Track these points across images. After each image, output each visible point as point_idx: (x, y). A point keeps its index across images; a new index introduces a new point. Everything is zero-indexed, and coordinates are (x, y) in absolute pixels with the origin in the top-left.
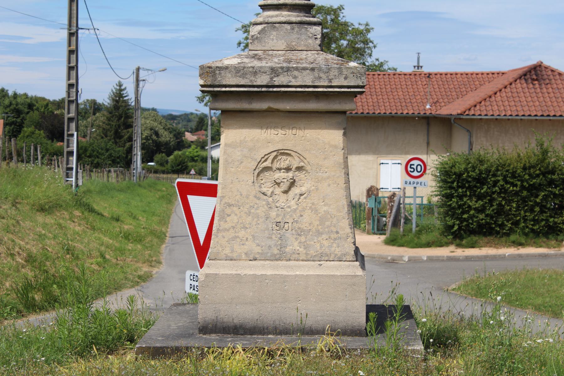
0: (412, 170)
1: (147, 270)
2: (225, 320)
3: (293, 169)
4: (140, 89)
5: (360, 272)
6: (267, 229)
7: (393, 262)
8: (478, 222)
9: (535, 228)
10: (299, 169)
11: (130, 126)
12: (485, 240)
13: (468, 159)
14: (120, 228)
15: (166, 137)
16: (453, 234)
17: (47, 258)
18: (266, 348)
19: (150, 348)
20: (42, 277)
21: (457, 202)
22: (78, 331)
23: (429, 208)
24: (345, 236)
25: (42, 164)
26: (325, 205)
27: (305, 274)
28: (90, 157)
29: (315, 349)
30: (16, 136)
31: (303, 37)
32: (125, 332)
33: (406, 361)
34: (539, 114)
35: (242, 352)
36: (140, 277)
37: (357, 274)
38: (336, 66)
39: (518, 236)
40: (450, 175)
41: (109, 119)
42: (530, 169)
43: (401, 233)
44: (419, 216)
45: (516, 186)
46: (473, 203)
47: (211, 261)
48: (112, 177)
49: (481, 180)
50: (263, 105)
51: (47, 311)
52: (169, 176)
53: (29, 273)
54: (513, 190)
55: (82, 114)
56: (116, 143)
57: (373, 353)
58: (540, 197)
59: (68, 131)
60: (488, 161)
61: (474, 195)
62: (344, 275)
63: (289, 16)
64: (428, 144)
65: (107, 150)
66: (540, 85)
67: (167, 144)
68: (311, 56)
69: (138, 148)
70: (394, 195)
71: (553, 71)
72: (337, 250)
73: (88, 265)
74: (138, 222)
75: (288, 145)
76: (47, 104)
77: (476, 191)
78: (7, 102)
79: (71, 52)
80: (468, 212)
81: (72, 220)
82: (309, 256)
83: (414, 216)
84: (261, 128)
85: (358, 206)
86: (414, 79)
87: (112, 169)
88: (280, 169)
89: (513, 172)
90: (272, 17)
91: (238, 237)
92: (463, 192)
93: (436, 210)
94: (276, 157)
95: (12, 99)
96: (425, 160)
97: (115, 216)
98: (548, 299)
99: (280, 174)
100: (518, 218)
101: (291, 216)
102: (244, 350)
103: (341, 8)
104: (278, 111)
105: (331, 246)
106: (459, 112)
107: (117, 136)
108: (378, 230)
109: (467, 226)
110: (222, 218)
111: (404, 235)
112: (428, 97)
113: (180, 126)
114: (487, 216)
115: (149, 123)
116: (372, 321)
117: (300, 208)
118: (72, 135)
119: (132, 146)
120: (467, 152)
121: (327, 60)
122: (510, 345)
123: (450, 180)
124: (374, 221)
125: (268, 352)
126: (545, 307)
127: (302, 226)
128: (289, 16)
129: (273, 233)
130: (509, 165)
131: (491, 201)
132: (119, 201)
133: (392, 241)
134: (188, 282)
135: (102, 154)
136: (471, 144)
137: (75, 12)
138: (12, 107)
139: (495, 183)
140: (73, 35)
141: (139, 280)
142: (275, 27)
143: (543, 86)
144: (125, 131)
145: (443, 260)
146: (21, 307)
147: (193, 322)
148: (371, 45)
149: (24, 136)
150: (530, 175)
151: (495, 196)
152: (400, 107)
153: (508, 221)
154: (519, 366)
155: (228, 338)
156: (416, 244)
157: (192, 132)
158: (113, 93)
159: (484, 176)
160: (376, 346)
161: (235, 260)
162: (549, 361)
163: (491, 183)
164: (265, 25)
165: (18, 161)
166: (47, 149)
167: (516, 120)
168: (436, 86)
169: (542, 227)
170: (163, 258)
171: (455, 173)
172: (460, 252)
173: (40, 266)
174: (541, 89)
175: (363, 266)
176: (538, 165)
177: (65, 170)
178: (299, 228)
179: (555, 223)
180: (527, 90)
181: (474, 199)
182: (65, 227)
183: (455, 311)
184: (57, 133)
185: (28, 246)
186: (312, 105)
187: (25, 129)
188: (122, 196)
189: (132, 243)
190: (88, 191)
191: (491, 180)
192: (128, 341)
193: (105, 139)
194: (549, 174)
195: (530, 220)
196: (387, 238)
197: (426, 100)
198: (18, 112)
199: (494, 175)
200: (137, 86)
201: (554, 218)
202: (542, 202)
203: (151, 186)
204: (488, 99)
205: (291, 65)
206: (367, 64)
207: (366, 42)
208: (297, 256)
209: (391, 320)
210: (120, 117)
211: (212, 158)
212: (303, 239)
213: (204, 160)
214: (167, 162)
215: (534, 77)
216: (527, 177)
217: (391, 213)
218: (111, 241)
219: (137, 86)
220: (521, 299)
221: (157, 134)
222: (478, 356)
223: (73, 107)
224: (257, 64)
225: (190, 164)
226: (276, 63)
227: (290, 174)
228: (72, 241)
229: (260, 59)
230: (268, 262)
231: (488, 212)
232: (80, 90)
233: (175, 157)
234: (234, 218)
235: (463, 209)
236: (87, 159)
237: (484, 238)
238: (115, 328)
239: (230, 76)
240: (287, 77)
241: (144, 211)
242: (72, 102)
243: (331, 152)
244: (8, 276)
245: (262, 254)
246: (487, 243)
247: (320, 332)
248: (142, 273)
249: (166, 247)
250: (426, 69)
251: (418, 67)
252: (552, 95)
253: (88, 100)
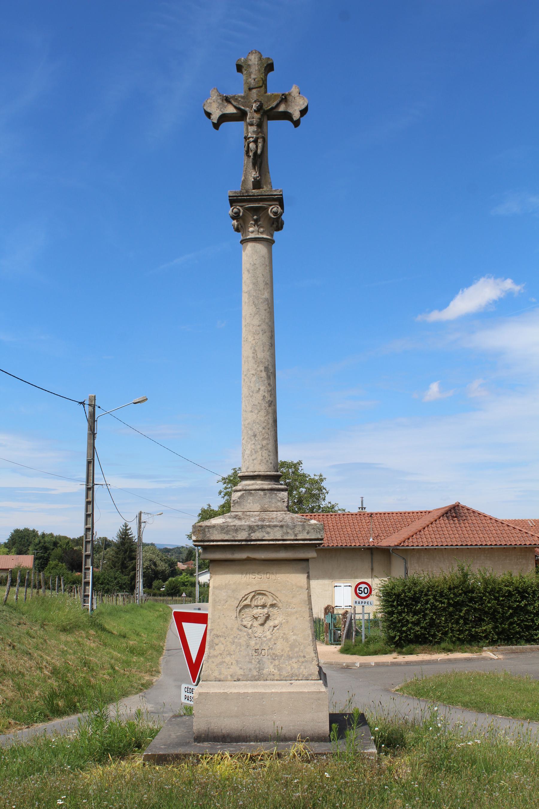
0: (360, 592)
1: (148, 678)
2: (215, 730)
3: (268, 606)
4: (142, 529)
5: (323, 689)
6: (248, 655)
7: (348, 667)
8: (414, 633)
9: (461, 637)
10: (272, 606)
11: (135, 559)
12: (421, 647)
13: (404, 583)
14: (127, 643)
15: (162, 566)
16: (395, 643)
17: (68, 670)
18: (249, 754)
19: (155, 755)
20: (65, 687)
21: (397, 618)
22: (96, 740)
23: (375, 622)
24: (310, 659)
25: (65, 590)
26: (294, 635)
27: (279, 691)
28: (102, 584)
30: (43, 568)
31: (274, 501)
32: (134, 739)
33: (363, 764)
35: (230, 758)
36: (143, 685)
37: (321, 690)
38: (300, 523)
39: (447, 644)
40: (390, 596)
41: (117, 553)
42: (454, 589)
45: (444, 603)
47: (203, 682)
48: (119, 600)
49: (415, 599)
50: (243, 555)
51: (68, 715)
52: (165, 598)
53: (54, 683)
54: (442, 607)
55: (96, 549)
56: (122, 572)
57: (336, 757)
58: (463, 612)
59: (85, 565)
60: (421, 583)
61: (411, 611)
62: (311, 692)
64: (372, 569)
65: (116, 578)
67: (163, 572)
68: (280, 515)
69: (141, 576)
70: (346, 612)
71: (468, 509)
72: (305, 671)
73: (101, 675)
74: (140, 638)
75: (263, 587)
77: (412, 608)
78: (37, 541)
79: (88, 503)
81: (88, 637)
82: (282, 677)
83: (363, 629)
84: (242, 573)
85: (317, 622)
86: (359, 518)
87: (120, 594)
88: (257, 606)
89: (441, 592)
90: (249, 485)
92: (401, 609)
93: (381, 624)
94: (254, 596)
95: (41, 538)
96: (370, 583)
97: (122, 634)
98: (473, 697)
99: (257, 610)
100: (447, 629)
101: (267, 644)
102: (231, 756)
103: (300, 463)
104: (255, 559)
105: (300, 668)
106: (396, 544)
107: (124, 566)
108: (334, 641)
109: (406, 636)
110: (212, 647)
111: (356, 645)
112: (371, 532)
113: (173, 557)
114: (421, 628)
115: (149, 555)
116: (334, 730)
117: (274, 638)
118: (89, 569)
121: (292, 519)
122: (447, 747)
126: (472, 704)
127: (276, 653)
128: (262, 484)
129: (253, 658)
130: (438, 586)
131: (425, 616)
132: (125, 621)
133: (346, 650)
134: (183, 694)
138: (41, 545)
139: (427, 601)
140: (90, 489)
141: (142, 688)
142: (251, 493)
143: (461, 521)
144: (130, 562)
146: (47, 712)
149: (49, 568)
150: (454, 594)
151: (428, 612)
152: (349, 541)
153: (438, 632)
154: (455, 765)
155: (218, 745)
156: (366, 652)
157: (184, 562)
158: (121, 532)
159: (417, 595)
161: (222, 681)
162: (478, 759)
163: (424, 601)
164: (244, 492)
165: (45, 589)
167: (441, 550)
169: (466, 636)
170: (161, 668)
171: (395, 594)
172: (402, 659)
173: (63, 677)
175: (326, 684)
176: (460, 586)
177: (82, 596)
178: (274, 654)
179: (476, 632)
181: (411, 615)
182: (83, 644)
184: (76, 565)
185: (53, 661)
187: (51, 562)
189: (136, 656)
190: (101, 613)
191: (424, 599)
192: (136, 747)
194: (469, 593)
196: (341, 648)
197: (369, 535)
198: (45, 549)
199: (426, 595)
200: (140, 527)
201: (476, 628)
202: (465, 616)
203: (151, 608)
204: (418, 533)
205: (264, 523)
206: (322, 506)
207: (320, 489)
208: (272, 677)
209: (350, 730)
211: (199, 582)
212: (277, 662)
213: (193, 585)
215: (454, 515)
216: (452, 596)
217: (344, 627)
219: (140, 527)
220: (452, 697)
221: (155, 564)
222: (421, 758)
223: (89, 546)
224: (237, 523)
225: (182, 588)
226: (252, 522)
227: (266, 610)
228: (88, 656)
229: (240, 519)
230: (249, 682)
232: (95, 533)
233: (170, 583)
234: (221, 647)
235: (402, 623)
237: (420, 646)
238: (126, 737)
239: (216, 532)
240: (261, 533)
241: (146, 629)
242: (89, 542)
243: (298, 591)
245: (244, 675)
246: (423, 650)
247: (292, 739)
248: (145, 681)
249: (164, 658)
250: (368, 510)
251: (362, 508)
252: (468, 528)
253: (100, 538)
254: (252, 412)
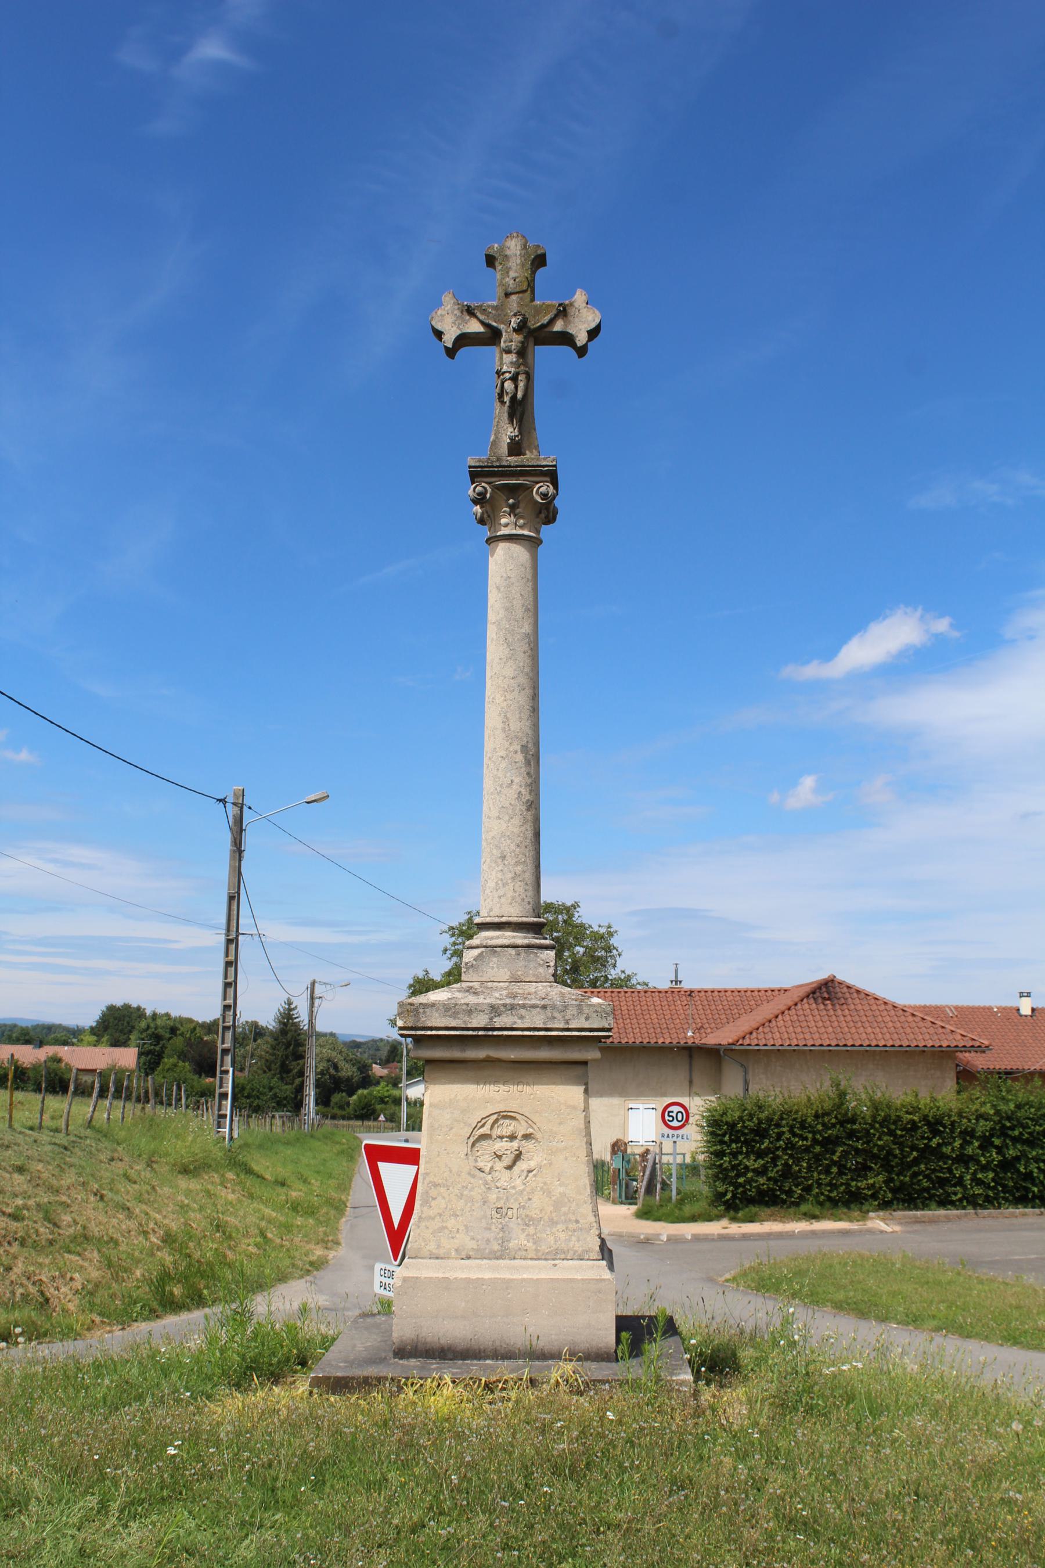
2: (429, 1340)
4: (315, 1010)
5: (607, 1275)
7: (646, 1242)
9: (832, 1195)
10: (527, 1137)
12: (768, 1211)
14: (287, 1195)
15: (347, 1070)
16: (726, 1203)
17: (191, 1237)
19: (329, 1378)
20: (184, 1264)
21: (730, 1162)
23: (693, 1169)
25: (187, 1107)
26: (560, 1185)
27: (535, 1277)
28: (248, 1097)
29: (548, 1382)
31: (532, 965)
32: (295, 1351)
33: (670, 1399)
34: (833, 1044)
36: (311, 1263)
38: (574, 1002)
39: (810, 1206)
40: (720, 1126)
41: (274, 1048)
43: (657, 1203)
44: (680, 1178)
45: (806, 1139)
46: (752, 1163)
48: (277, 1124)
49: (760, 1133)
50: (481, 1054)
51: (189, 1310)
52: (351, 1122)
53: (167, 1257)
58: (838, 1154)
59: (222, 1066)
60: (770, 1106)
61: (753, 1152)
63: (514, 937)
64: (691, 1082)
65: (271, 1089)
66: (833, 1005)
67: (349, 1080)
68: (542, 989)
70: (647, 1151)
72: (577, 1245)
73: (244, 1246)
75: (512, 1106)
76: (195, 1027)
78: (143, 1024)
79: (228, 964)
80: (744, 1175)
82: (540, 1254)
83: (674, 1179)
84: (478, 1083)
85: (599, 1166)
87: (277, 1114)
88: (501, 1137)
90: (492, 938)
91: (446, 1228)
93: (703, 1172)
94: (496, 1121)
95: (150, 1021)
98: (852, 1294)
100: (810, 1182)
101: (516, 1200)
102: (454, 1382)
103: (576, 905)
104: (499, 1060)
106: (731, 1041)
107: (284, 1069)
108: (627, 1198)
109: (744, 1192)
111: (661, 1206)
113: (366, 1055)
115: (326, 1052)
118: (227, 1072)
119: (303, 1082)
120: (742, 1095)
121: (562, 995)
123: (719, 1132)
124: (621, 1186)
125: (486, 1385)
128: (514, 937)
130: (797, 1112)
131: (775, 1159)
133: (646, 1213)
134: (377, 1279)
135: (264, 1094)
136: (746, 1083)
137: (235, 912)
139: (779, 1136)
140: (232, 942)
143: (838, 1007)
144: (294, 1063)
145: (713, 1240)
146: (155, 1305)
147: (385, 1341)
148: (614, 952)
150: (824, 1125)
153: (797, 1186)
154: (820, 1402)
156: (677, 1218)
159: (763, 1126)
160: (630, 1377)
166: (192, 1087)
168: (700, 1007)
170: (342, 1237)
174: (835, 1011)
175: (611, 1267)
177: (216, 1117)
178: (527, 1216)
179: (858, 1188)
180: (816, 1012)
181: (752, 1157)
182: (215, 1195)
183: (731, 1322)
184: (207, 1066)
186: (544, 1054)
187: (166, 1060)
188: (289, 1151)
189: (301, 1216)
191: (773, 1132)
192: (299, 1364)
193: (269, 1074)
195: (826, 1185)
196: (638, 1209)
198: (157, 1038)
199: (778, 1125)
201: (857, 1181)
203: (327, 1137)
205: (516, 1002)
206: (610, 977)
207: (608, 949)
209: (650, 1342)
210: (288, 1045)
212: (531, 1230)
213: (397, 1101)
214: (348, 1104)
215: (826, 995)
216: (820, 1127)
218: (274, 1214)
220: (817, 1293)
221: (336, 1067)
223: (229, 1035)
224: (471, 999)
225: (378, 1107)
227: (515, 1144)
229: (476, 993)
230: (485, 1261)
231: (770, 1175)
232: (238, 1013)
233: (359, 1098)
234: (441, 1203)
236: (244, 1100)
237: (766, 1209)
240: (511, 1017)
241: (318, 1172)
242: (228, 1028)
243: (568, 1114)
244: (139, 1261)
245: (478, 1250)
248: (315, 1258)
250: (686, 985)
251: (676, 982)
253: (247, 1022)
254: (499, 818)
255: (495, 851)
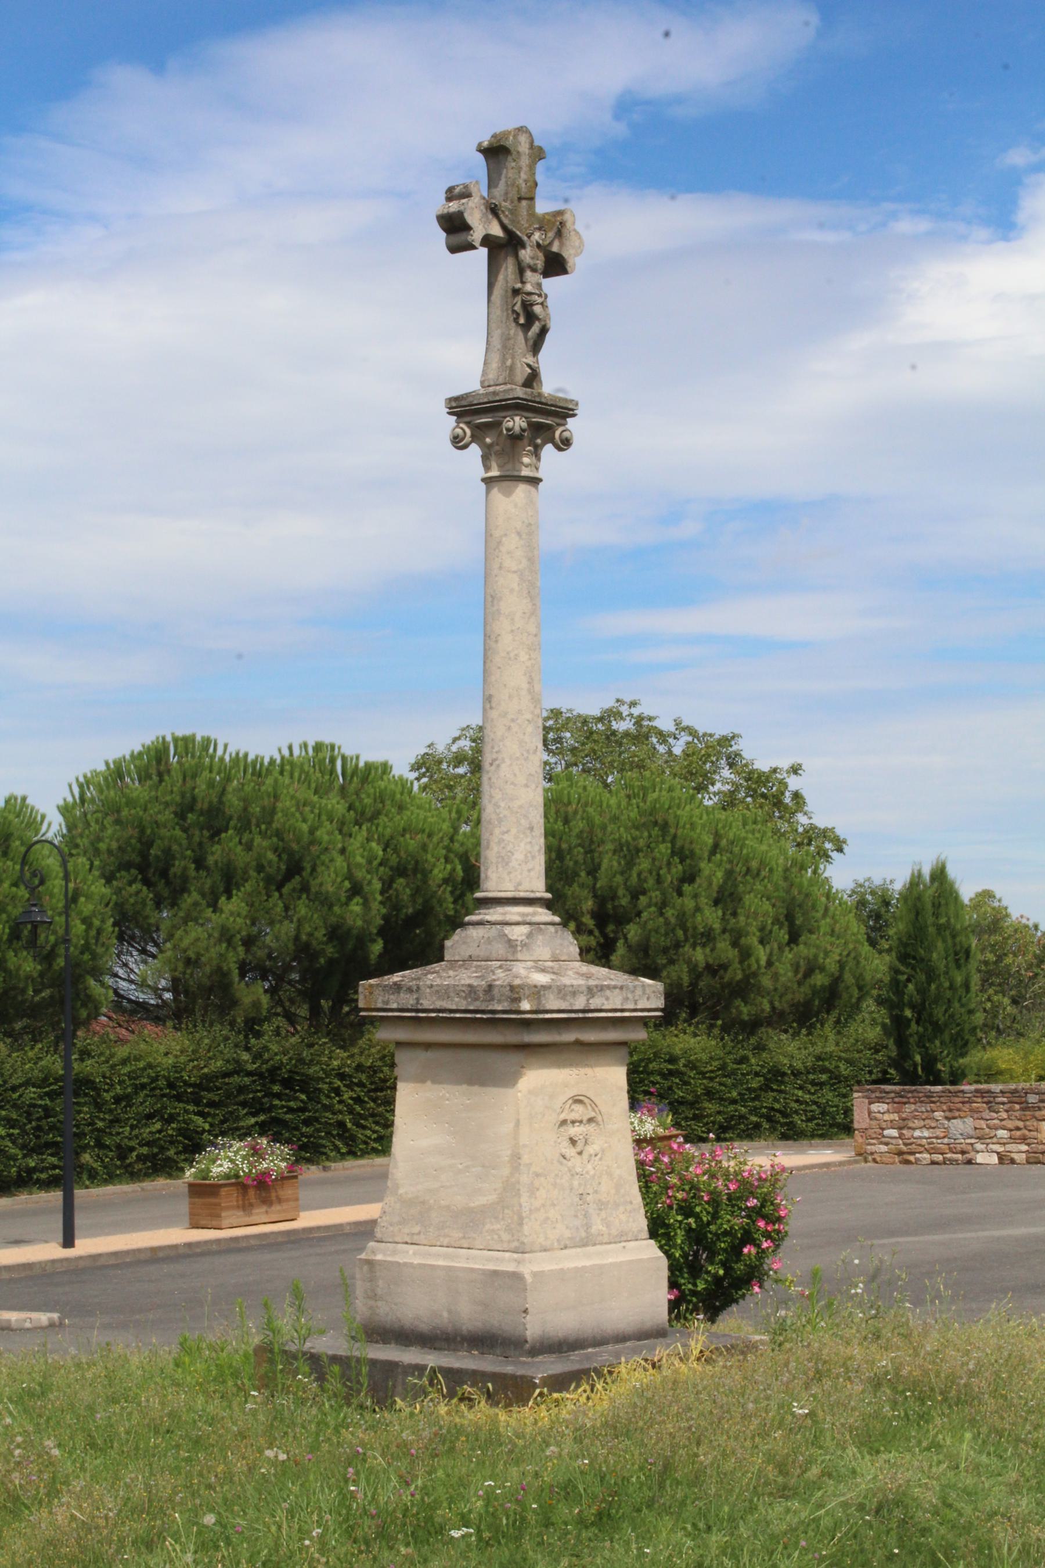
142: (541, 929)
234: (542, 1193)
254: (527, 786)
255: (523, 821)
